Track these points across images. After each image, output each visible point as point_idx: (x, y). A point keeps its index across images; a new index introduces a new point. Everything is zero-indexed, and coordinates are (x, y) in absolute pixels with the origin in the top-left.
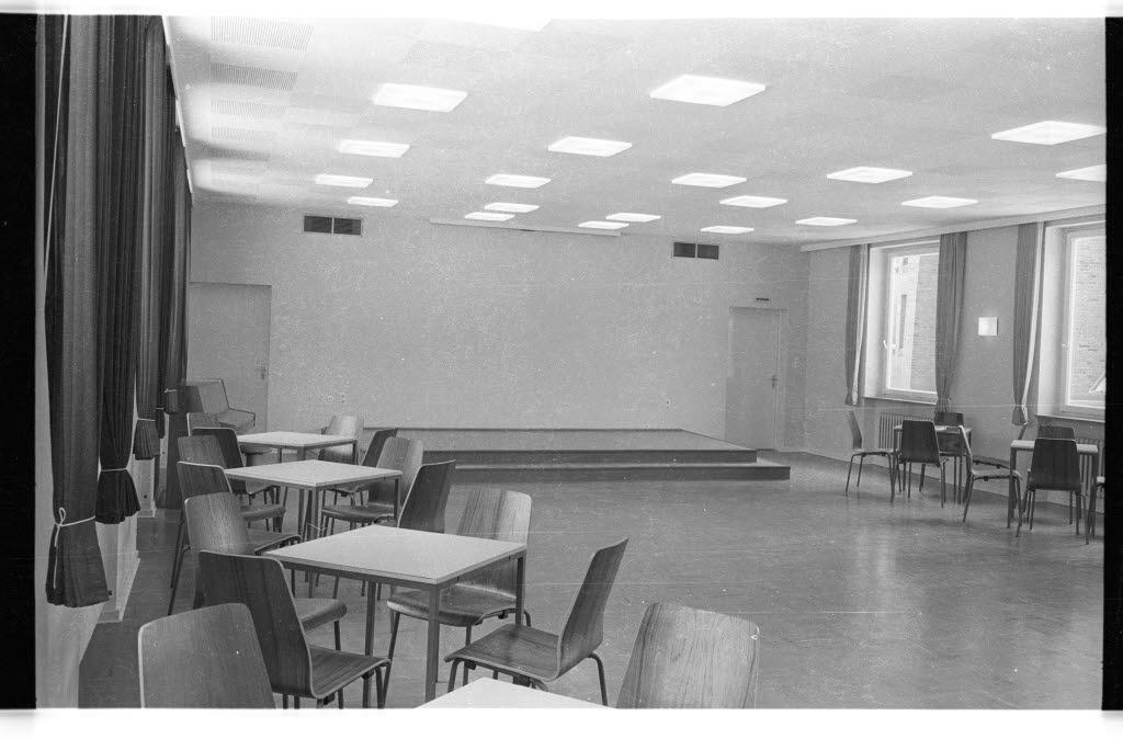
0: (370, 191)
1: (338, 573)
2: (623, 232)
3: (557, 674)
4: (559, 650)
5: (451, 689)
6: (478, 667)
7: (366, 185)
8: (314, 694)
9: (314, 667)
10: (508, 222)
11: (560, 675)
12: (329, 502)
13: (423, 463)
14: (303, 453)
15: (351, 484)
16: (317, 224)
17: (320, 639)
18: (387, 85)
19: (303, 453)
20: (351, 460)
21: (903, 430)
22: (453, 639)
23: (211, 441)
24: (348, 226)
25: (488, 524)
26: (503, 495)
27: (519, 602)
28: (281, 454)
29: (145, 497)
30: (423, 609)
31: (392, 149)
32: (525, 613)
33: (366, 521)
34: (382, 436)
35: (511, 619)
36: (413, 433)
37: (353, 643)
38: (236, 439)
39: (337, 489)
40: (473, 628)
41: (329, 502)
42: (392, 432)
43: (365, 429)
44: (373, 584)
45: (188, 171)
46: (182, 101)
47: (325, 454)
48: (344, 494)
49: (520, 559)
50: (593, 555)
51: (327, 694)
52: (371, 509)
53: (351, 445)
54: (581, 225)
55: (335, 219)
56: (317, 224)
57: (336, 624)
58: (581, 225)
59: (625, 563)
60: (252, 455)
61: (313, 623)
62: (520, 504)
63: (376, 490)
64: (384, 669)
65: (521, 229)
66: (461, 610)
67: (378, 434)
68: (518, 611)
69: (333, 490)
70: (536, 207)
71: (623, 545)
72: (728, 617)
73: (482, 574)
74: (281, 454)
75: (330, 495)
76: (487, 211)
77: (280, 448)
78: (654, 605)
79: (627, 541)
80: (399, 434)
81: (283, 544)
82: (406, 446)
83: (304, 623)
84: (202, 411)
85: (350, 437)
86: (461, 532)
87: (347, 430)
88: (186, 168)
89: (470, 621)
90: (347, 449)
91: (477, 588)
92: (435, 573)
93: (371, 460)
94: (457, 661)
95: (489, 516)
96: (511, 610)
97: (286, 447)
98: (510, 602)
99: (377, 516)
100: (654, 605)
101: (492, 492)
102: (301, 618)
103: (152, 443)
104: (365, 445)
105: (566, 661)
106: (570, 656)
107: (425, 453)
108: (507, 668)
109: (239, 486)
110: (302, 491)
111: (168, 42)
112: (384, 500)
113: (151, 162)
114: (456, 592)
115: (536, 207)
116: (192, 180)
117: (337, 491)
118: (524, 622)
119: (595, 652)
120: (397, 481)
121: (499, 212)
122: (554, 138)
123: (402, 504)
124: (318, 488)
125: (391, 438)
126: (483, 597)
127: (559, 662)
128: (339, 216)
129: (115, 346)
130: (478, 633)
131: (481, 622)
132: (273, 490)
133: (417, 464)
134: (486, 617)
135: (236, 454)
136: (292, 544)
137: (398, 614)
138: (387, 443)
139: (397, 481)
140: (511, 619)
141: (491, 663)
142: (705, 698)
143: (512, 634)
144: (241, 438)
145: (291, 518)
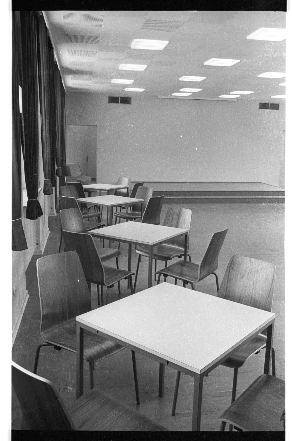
0: (134, 85)
1: (120, 241)
2: (238, 99)
3: (198, 280)
4: (199, 271)
5: (158, 283)
6: (168, 276)
7: (131, 83)
8: (105, 284)
9: (105, 275)
10: (189, 96)
11: (199, 281)
12: (119, 211)
13: (153, 196)
14: (109, 192)
15: (126, 204)
16: (114, 100)
17: (111, 264)
18: (136, 40)
19: (109, 192)
20: (126, 195)
21: (43, 331)
22: (161, 265)
23: (73, 188)
24: (126, 100)
25: (175, 222)
26: (180, 210)
27: (186, 251)
28: (100, 192)
29: (52, 208)
30: (148, 253)
31: (140, 67)
32: (188, 255)
33: (131, 219)
34: (138, 185)
35: (183, 257)
36: (147, 184)
37: (123, 267)
38: (82, 187)
39: (120, 206)
40: (168, 261)
41: (119, 211)
42: (141, 184)
43: (132, 182)
44: (131, 245)
45: (62, 80)
46: (57, 50)
47: (116, 192)
48: (124, 208)
49: (186, 235)
50: (213, 235)
51: (111, 284)
52: (133, 214)
53: (126, 189)
54: (220, 97)
55: (121, 98)
56: (114, 100)
57: (117, 258)
58: (220, 97)
59: (227, 236)
60: (91, 193)
61: (104, 259)
62: (187, 214)
63: (135, 207)
64: (133, 277)
65: (195, 99)
66: (165, 254)
67: (136, 185)
68: (185, 255)
69: (120, 207)
70: (201, 90)
71: (226, 231)
72: (264, 262)
73: (172, 241)
74: (100, 192)
75: (119, 208)
76: (181, 92)
77: (100, 190)
78: (234, 256)
79: (227, 229)
80: (145, 185)
81: (99, 227)
82: (146, 190)
83: (101, 259)
84: (71, 176)
85: (126, 186)
86: (164, 225)
87: (125, 183)
88: (61, 78)
89: (167, 259)
90: (125, 191)
91: (171, 246)
92: (151, 241)
93: (133, 196)
94: (161, 274)
95: (175, 218)
96: (183, 255)
97: (101, 190)
98: (182, 251)
99: (135, 217)
100: (234, 256)
101: (176, 208)
102: (100, 256)
103: (50, 189)
104: (132, 188)
105: (202, 276)
106: (204, 273)
107: (154, 192)
108: (181, 278)
109: (84, 205)
110: (108, 208)
111: (47, 26)
112: (138, 211)
113: (44, 77)
114: (164, 247)
115: (201, 90)
116: (64, 83)
117: (121, 207)
118: (188, 260)
119: (214, 272)
120: (142, 203)
121: (186, 92)
122: (207, 59)
123: (144, 212)
124: (112, 206)
125: (140, 187)
126: (172, 249)
127: (199, 276)
128: (123, 96)
129: (30, 153)
130: (170, 263)
131: (171, 259)
132: (98, 207)
133: (150, 195)
134: (173, 257)
135: (82, 192)
136: (103, 227)
137: (140, 255)
138: (138, 189)
139: (142, 203)
140: (183, 258)
141: (175, 276)
142: (253, 293)
143: (183, 264)
144: (84, 186)
145: (104, 216)
